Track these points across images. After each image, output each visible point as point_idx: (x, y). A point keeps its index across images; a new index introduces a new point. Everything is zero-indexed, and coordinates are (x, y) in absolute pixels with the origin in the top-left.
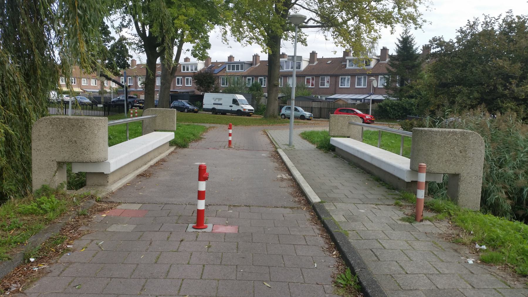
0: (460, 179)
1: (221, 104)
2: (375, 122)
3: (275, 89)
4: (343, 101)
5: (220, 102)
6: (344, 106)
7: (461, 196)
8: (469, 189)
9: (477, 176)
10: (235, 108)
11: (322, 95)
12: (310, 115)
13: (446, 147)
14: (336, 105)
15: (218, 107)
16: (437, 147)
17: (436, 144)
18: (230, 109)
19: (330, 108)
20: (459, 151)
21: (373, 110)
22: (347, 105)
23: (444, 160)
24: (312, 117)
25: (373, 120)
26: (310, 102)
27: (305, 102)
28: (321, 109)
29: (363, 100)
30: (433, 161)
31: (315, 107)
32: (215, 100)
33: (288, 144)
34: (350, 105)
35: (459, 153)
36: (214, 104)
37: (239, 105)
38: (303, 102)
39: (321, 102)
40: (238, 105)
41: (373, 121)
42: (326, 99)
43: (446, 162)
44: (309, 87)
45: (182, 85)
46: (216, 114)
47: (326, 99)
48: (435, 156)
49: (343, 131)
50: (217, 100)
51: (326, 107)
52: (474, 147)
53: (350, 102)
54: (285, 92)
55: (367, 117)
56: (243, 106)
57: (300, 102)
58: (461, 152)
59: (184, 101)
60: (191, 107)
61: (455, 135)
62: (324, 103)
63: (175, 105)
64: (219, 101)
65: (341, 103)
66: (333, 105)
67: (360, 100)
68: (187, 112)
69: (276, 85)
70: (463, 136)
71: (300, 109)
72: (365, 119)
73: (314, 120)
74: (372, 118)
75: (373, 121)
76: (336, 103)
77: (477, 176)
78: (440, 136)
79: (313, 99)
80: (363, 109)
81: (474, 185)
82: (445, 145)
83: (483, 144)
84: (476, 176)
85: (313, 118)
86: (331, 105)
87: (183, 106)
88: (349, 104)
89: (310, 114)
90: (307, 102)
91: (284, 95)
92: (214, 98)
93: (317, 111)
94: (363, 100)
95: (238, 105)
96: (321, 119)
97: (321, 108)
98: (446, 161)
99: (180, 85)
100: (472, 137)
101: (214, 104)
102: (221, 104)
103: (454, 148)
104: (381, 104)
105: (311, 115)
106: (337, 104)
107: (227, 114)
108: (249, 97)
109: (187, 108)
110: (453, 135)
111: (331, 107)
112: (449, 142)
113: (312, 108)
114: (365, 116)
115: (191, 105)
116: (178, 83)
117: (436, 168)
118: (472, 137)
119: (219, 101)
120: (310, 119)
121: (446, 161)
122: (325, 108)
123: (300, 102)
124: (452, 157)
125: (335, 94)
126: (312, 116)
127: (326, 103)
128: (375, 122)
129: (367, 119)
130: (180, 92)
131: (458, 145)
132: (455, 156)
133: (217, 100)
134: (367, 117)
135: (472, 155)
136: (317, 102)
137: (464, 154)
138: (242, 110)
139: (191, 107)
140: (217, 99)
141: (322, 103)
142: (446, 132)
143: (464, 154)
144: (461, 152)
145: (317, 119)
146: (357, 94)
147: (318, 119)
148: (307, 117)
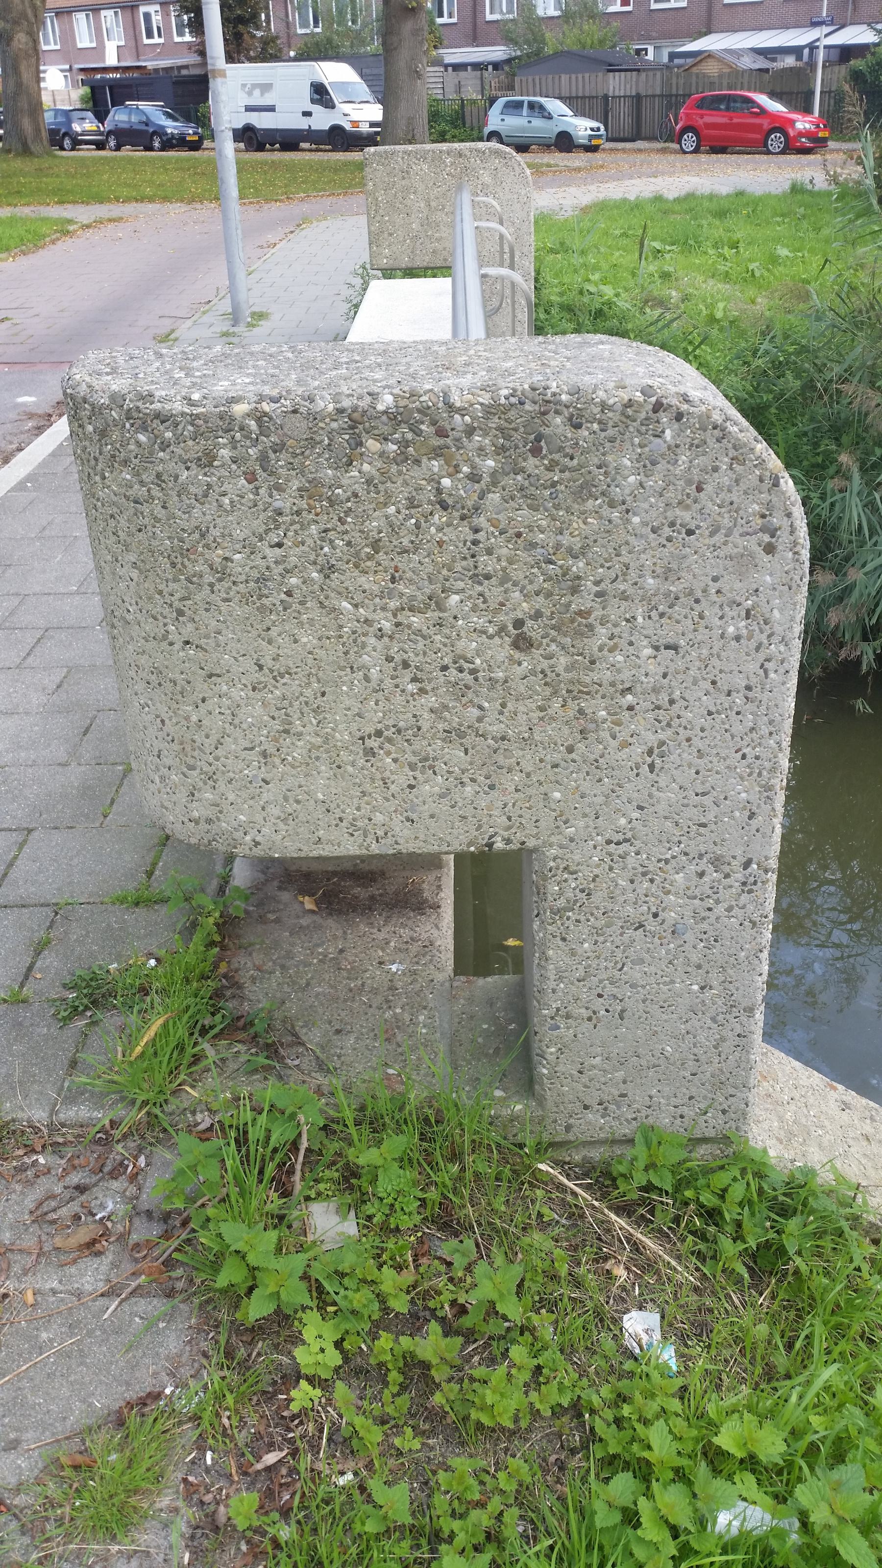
0: (542, 894)
1: (271, 109)
2: (831, 144)
3: (408, 26)
4: (720, 60)
5: (267, 101)
6: (725, 84)
7: (565, 1032)
8: (634, 973)
9: (717, 862)
10: (322, 120)
11: (659, 43)
12: (592, 129)
13: (347, 595)
14: (694, 78)
15: (263, 122)
16: (246, 599)
17: (222, 573)
18: (302, 124)
19: (671, 96)
20: (502, 629)
21: (830, 92)
22: (737, 76)
23: (343, 737)
24: (599, 137)
25: (821, 135)
26: (600, 74)
27: (580, 76)
28: (638, 99)
29: (806, 51)
30: (230, 745)
31: (617, 94)
32: (250, 93)
33: (230, 310)
34: (746, 76)
35: (501, 650)
36: (249, 109)
37: (333, 107)
38: (573, 76)
39: (638, 70)
40: (329, 104)
41: (825, 140)
42: (672, 56)
43: (370, 753)
44: (612, 9)
45: (162, 41)
46: (261, 148)
47: (672, 56)
48: (238, 694)
49: (438, 240)
50: (257, 92)
51: (658, 92)
52: (667, 574)
53: (748, 63)
54: (521, 40)
55: (799, 126)
56: (347, 108)
57: (563, 76)
58: (523, 643)
59: (144, 105)
60: (172, 127)
61: (437, 453)
62: (651, 73)
63: (121, 126)
64: (262, 94)
65: (711, 69)
66: (682, 81)
67: (796, 51)
68: (162, 149)
69: (413, 9)
70: (531, 464)
71: (555, 106)
72: (792, 133)
73: (611, 150)
74: (818, 126)
75: (825, 140)
76: (695, 70)
77: (717, 862)
78: (251, 478)
79: (612, 61)
80: (791, 93)
81: (689, 936)
82: (328, 570)
83: (784, 537)
84: (703, 865)
85: (608, 140)
86: (674, 81)
87: (144, 128)
88: (744, 71)
89: (595, 124)
90: (587, 75)
91: (519, 53)
92: (244, 86)
93: (622, 114)
94: (806, 51)
95: (329, 104)
96: (640, 144)
97: (638, 98)
98: (373, 743)
99: (157, 40)
100: (647, 464)
101: (249, 109)
102: (271, 109)
103: (436, 602)
104: (857, 63)
105: (598, 129)
106: (697, 75)
107: (303, 145)
108: (375, 71)
109: (160, 132)
110: (402, 458)
111: (674, 92)
112: (376, 545)
113: (606, 97)
114: (792, 122)
115: (175, 119)
116: (150, 35)
117: (275, 811)
118: (647, 464)
119: (262, 94)
120: (591, 149)
121: (373, 743)
122: (654, 96)
123: (563, 76)
124: (432, 701)
125: (708, 32)
126: (602, 131)
127: (658, 74)
128: (831, 144)
129: (801, 134)
130: (156, 70)
131: (488, 564)
132: (460, 691)
133: (257, 92)
134: (803, 124)
135: (651, 667)
136: (623, 74)
137: (563, 661)
138: (348, 127)
139: (172, 127)
140: (254, 86)
141: (643, 75)
142: (314, 417)
143: (563, 661)
144: (523, 643)
145: (621, 145)
146: (786, 27)
147: (628, 145)
148: (583, 138)
